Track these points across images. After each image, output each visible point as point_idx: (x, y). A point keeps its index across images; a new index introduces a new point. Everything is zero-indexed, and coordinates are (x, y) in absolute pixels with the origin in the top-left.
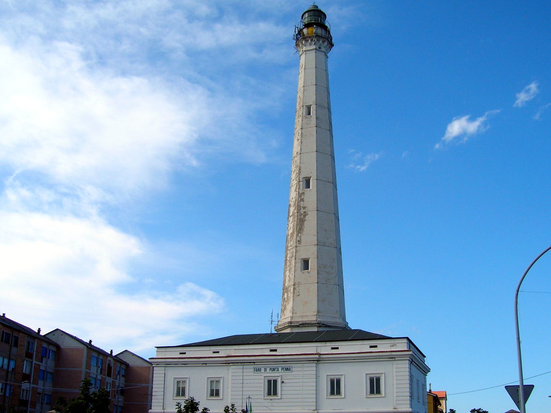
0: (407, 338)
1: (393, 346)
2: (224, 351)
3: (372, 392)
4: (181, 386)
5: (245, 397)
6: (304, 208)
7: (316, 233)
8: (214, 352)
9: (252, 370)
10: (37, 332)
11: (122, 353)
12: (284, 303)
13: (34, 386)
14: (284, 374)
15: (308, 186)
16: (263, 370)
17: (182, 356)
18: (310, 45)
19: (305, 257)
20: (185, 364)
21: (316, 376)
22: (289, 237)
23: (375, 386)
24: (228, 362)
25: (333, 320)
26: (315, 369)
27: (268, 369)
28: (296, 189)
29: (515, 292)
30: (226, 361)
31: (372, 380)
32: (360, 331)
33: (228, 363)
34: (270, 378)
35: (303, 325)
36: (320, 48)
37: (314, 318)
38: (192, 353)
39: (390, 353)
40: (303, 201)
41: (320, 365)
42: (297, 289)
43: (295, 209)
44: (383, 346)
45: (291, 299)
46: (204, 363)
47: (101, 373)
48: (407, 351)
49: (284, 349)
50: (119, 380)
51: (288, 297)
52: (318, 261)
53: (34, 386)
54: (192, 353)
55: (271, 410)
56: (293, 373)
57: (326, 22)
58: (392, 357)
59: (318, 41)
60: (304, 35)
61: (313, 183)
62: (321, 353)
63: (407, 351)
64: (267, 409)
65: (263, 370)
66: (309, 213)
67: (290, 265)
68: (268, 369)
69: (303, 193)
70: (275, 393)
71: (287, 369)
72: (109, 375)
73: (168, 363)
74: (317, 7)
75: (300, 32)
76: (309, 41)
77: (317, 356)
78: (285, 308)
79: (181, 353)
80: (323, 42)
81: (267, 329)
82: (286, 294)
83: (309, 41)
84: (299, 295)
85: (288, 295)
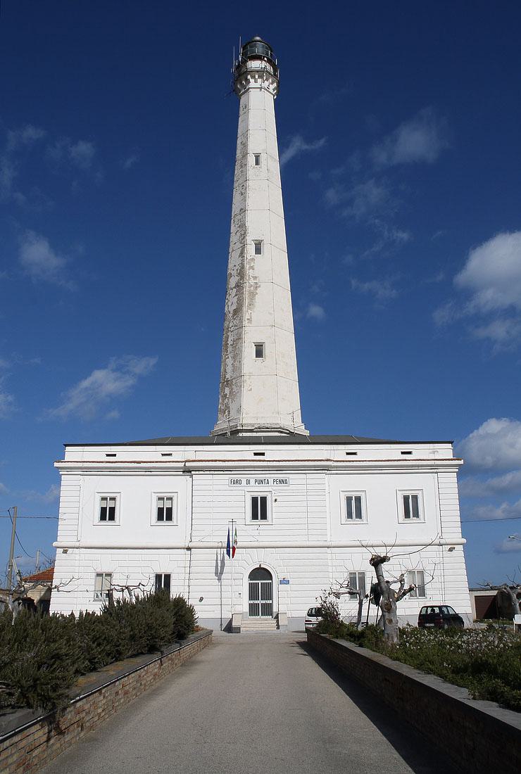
6: (255, 278)
9: (227, 482)
10: (74, 598)
13: (256, 602)
16: (244, 482)
23: (411, 507)
27: (252, 481)
34: (255, 495)
48: (452, 460)
53: (256, 602)
63: (452, 460)
65: (244, 482)
68: (252, 481)
71: (282, 482)
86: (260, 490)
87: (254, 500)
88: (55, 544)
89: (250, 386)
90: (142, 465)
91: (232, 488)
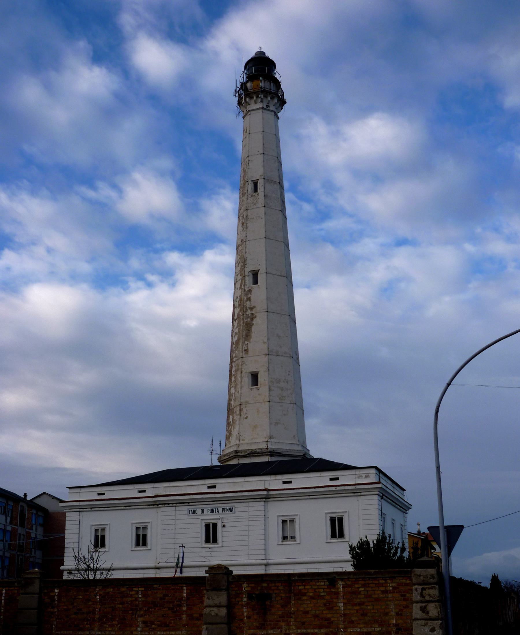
0: (376, 468)
1: (359, 477)
2: (152, 489)
3: (333, 536)
4: (141, 533)
5: (177, 546)
6: (251, 309)
7: (266, 340)
8: (140, 492)
9: (186, 512)
11: (39, 496)
12: (229, 427)
14: (226, 516)
15: (256, 282)
16: (199, 511)
17: (106, 496)
18: (256, 103)
19: (253, 369)
20: (106, 508)
21: (265, 518)
22: (234, 346)
24: (156, 503)
25: (288, 447)
26: (262, 508)
27: (206, 511)
28: (241, 286)
29: (445, 385)
30: (154, 501)
31: (333, 520)
32: (321, 460)
33: (156, 504)
34: (208, 522)
35: (252, 454)
36: (268, 106)
37: (264, 446)
38: (112, 493)
39: (354, 487)
40: (250, 300)
41: (269, 503)
42: (245, 410)
43: (240, 311)
44: (346, 478)
45: (237, 422)
46: (126, 505)
47: (11, 523)
49: (224, 485)
50: (36, 531)
51: (233, 420)
52: (269, 374)
54: (112, 493)
55: (210, 561)
56: (237, 514)
57: (275, 72)
58: (356, 491)
59: (266, 97)
60: (247, 90)
61: (261, 278)
62: (270, 488)
64: (205, 560)
65: (199, 511)
66: (258, 315)
67: (235, 381)
68: (206, 511)
69: (250, 291)
70: (215, 541)
71: (229, 510)
72: (22, 525)
73: (84, 507)
74: (264, 53)
75: (243, 87)
76: (255, 98)
77: (265, 493)
78: (231, 434)
79: (99, 494)
80: (272, 98)
81: (212, 460)
82: (231, 417)
83: (255, 98)
84: (246, 418)
85: (233, 417)
86: (211, 518)
87: (207, 526)
88: (62, 568)
89: (246, 413)
90: (406, 503)
91: (189, 517)
